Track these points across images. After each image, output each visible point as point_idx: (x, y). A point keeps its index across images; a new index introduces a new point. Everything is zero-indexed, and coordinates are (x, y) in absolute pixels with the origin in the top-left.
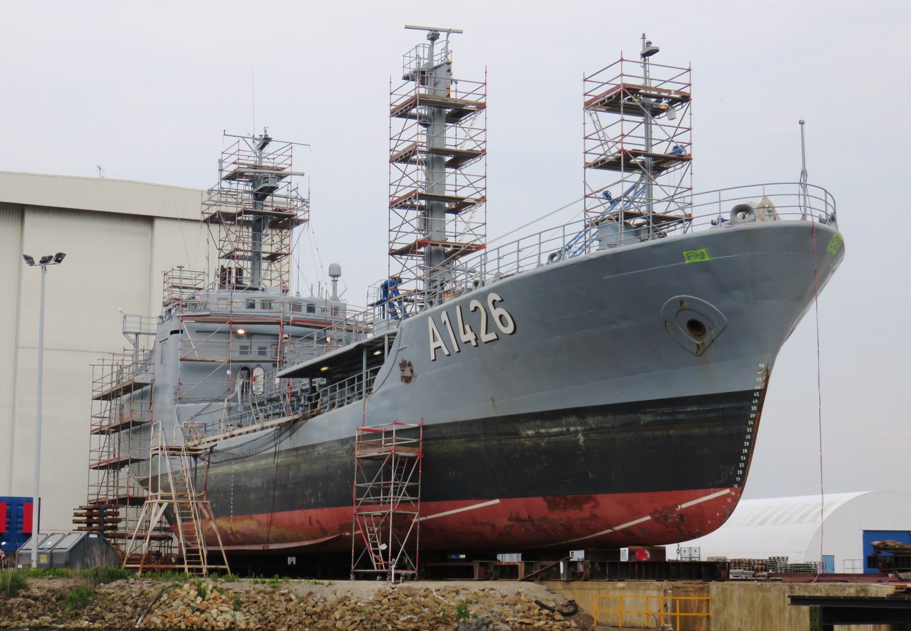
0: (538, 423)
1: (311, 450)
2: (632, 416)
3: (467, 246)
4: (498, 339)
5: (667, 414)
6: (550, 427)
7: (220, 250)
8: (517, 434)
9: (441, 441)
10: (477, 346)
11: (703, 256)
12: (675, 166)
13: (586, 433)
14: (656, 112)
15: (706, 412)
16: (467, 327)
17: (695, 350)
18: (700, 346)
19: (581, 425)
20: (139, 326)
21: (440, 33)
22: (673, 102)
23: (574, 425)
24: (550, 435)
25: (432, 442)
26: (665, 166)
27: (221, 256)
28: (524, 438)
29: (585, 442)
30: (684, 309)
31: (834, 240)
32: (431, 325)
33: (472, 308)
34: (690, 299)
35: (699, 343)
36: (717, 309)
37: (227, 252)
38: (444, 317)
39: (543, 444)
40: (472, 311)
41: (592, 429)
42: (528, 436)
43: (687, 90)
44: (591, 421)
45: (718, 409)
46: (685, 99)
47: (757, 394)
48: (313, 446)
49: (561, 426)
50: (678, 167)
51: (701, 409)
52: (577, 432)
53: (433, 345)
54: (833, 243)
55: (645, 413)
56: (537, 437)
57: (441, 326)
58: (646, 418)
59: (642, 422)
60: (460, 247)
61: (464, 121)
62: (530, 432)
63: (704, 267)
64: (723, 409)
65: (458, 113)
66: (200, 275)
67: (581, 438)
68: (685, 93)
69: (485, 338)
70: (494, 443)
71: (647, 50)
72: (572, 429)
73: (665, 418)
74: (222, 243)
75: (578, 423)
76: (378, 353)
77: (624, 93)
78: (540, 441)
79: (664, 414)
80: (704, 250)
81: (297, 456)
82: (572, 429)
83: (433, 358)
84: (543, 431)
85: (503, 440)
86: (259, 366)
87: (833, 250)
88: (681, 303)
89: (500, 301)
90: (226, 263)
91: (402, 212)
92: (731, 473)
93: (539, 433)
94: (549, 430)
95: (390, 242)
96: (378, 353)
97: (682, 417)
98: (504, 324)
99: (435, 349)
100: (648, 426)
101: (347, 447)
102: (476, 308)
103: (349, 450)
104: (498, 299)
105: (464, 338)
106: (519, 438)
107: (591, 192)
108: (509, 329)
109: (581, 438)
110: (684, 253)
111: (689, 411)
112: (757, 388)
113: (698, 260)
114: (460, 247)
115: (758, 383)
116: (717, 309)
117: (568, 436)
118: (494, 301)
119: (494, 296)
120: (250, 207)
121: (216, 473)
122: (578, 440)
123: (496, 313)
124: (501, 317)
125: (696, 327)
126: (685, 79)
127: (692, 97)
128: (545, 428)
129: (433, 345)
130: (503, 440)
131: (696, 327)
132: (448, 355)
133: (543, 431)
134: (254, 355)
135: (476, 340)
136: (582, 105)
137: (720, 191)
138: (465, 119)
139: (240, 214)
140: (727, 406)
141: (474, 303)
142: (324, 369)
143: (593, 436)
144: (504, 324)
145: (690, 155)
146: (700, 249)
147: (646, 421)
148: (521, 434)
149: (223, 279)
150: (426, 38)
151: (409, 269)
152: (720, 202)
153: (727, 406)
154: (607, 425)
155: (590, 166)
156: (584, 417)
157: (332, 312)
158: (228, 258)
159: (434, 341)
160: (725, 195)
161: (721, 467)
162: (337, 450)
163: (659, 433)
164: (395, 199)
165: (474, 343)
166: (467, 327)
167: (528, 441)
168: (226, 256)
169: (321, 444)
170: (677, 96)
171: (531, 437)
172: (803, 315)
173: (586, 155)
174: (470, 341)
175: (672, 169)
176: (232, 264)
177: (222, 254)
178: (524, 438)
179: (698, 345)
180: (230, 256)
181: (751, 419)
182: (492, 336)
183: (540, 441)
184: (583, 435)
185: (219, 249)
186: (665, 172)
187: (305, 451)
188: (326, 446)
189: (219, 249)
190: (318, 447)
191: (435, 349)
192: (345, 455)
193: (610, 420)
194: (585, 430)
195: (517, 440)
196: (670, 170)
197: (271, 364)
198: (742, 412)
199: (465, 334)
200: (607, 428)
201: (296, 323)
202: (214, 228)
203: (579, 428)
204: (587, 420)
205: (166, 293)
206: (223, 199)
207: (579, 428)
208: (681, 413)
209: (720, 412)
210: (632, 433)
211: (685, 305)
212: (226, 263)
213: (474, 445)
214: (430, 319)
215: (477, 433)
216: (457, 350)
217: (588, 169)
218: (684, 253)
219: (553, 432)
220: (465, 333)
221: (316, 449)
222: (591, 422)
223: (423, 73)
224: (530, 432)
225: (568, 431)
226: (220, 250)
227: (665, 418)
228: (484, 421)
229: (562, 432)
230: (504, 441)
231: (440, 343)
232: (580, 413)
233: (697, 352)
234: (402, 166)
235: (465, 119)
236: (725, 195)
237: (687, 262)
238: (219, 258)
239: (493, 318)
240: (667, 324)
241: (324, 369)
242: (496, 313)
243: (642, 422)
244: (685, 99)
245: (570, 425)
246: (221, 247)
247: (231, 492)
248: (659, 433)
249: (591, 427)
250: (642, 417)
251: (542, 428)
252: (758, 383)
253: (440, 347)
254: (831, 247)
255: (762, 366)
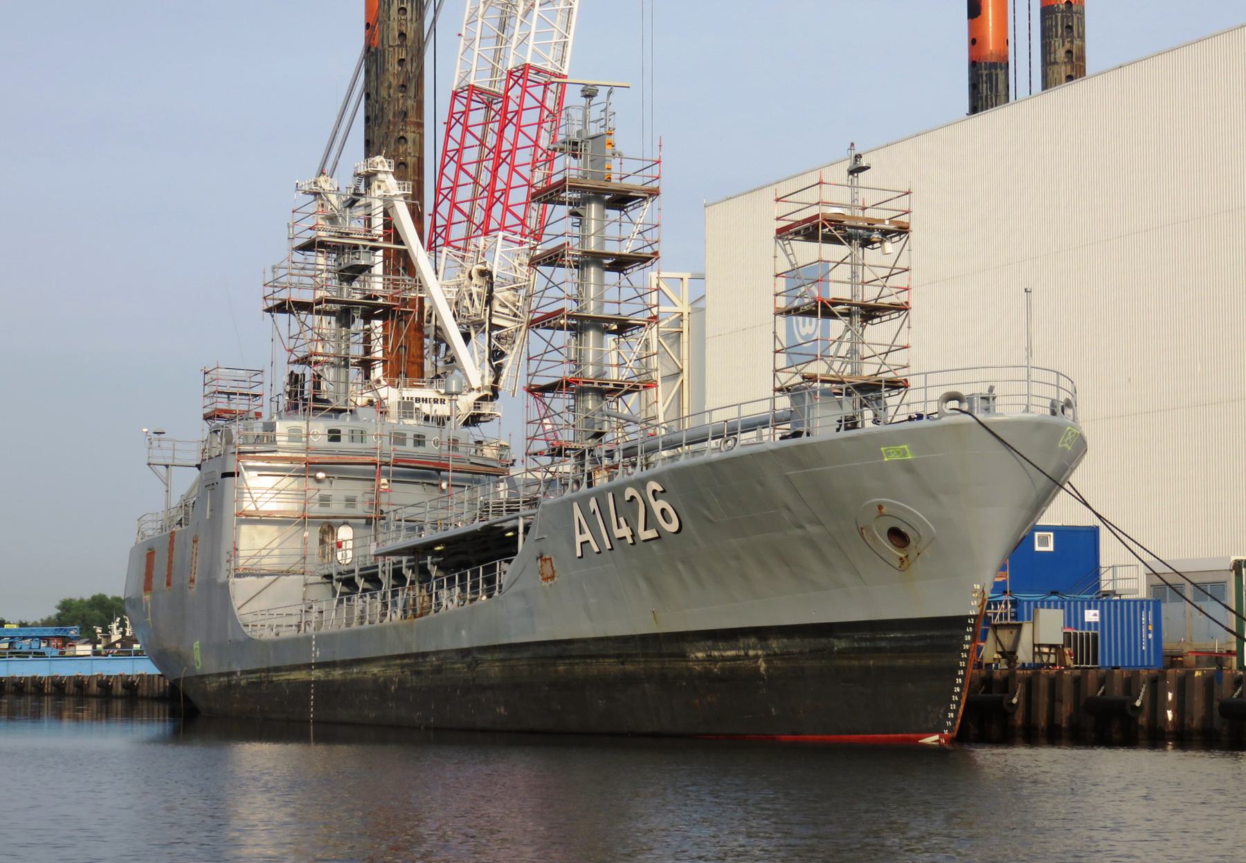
0: (710, 643)
1: (421, 660)
2: (824, 641)
3: (632, 384)
4: (659, 537)
5: (866, 640)
6: (725, 650)
7: (291, 351)
8: (683, 656)
9: (589, 661)
10: (634, 544)
11: (905, 454)
12: (890, 314)
13: (769, 658)
14: (866, 243)
15: (912, 639)
16: (622, 520)
17: (897, 564)
18: (904, 559)
19: (762, 648)
20: (172, 455)
21: (598, 87)
22: (885, 233)
23: (754, 648)
24: (724, 659)
25: (577, 661)
26: (878, 314)
27: (291, 360)
28: (693, 661)
29: (767, 670)
30: (882, 515)
31: (1067, 433)
32: (577, 513)
33: (627, 498)
34: (891, 504)
35: (902, 555)
36: (924, 518)
37: (301, 355)
38: (593, 505)
39: (716, 670)
40: (628, 501)
41: (775, 654)
42: (697, 660)
43: (905, 219)
44: (775, 644)
45: (926, 637)
46: (903, 230)
47: (971, 621)
48: (424, 655)
49: (739, 649)
50: (893, 316)
51: (906, 635)
52: (757, 657)
53: (579, 539)
54: (1065, 438)
55: (839, 638)
56: (708, 661)
57: (589, 516)
58: (840, 644)
59: (836, 649)
60: (623, 386)
61: (632, 207)
62: (700, 655)
63: (908, 467)
64: (931, 637)
65: (621, 200)
66: (256, 374)
67: (763, 666)
68: (903, 222)
69: (645, 535)
70: (656, 666)
71: (855, 167)
72: (751, 653)
73: (863, 644)
74: (293, 341)
75: (759, 646)
76: (510, 534)
77: (823, 224)
78: (712, 666)
79: (862, 640)
80: (905, 447)
81: (402, 666)
82: (751, 653)
83: (579, 554)
84: (716, 653)
85: (667, 663)
86: (345, 524)
87: (1067, 445)
88: (880, 507)
89: (661, 492)
90: (298, 369)
91: (547, 333)
92: (941, 716)
93: (710, 656)
94: (724, 654)
95: (529, 375)
96: (510, 534)
97: (883, 644)
98: (667, 519)
99: (582, 543)
100: (841, 652)
101: (469, 659)
102: (633, 498)
103: (471, 663)
104: (660, 489)
105: (618, 533)
106: (686, 661)
107: (781, 348)
108: (674, 527)
109: (763, 666)
110: (882, 449)
111: (891, 638)
112: (971, 613)
113: (898, 458)
114: (623, 386)
115: (972, 608)
116: (924, 518)
117: (746, 662)
118: (654, 492)
119: (654, 485)
120: (333, 295)
121: (289, 680)
122: (759, 667)
123: (657, 506)
124: (663, 511)
125: (898, 536)
126: (902, 203)
127: (912, 228)
128: (719, 650)
129: (579, 539)
130: (667, 663)
131: (898, 536)
132: (598, 553)
133: (716, 653)
134: (336, 508)
135: (633, 536)
136: (774, 233)
137: (926, 374)
138: (633, 205)
139: (319, 303)
140: (937, 633)
141: (630, 492)
142: (438, 548)
143: (777, 663)
144: (667, 519)
145: (907, 303)
146: (902, 444)
147: (840, 647)
148: (688, 656)
149: (293, 395)
150: (580, 94)
151: (557, 286)
152: (926, 387)
153: (937, 633)
154: (794, 650)
155: (781, 314)
156: (766, 639)
157: (449, 447)
158: (303, 363)
159: (580, 534)
160: (932, 379)
161: (929, 708)
162: (455, 663)
163: (855, 663)
164: (537, 316)
165: (630, 541)
166: (622, 520)
167: (698, 665)
168: (298, 361)
169: (436, 653)
170: (892, 227)
171: (701, 661)
172: (1043, 512)
173: (778, 297)
174: (625, 538)
175: (887, 318)
176: (309, 372)
177: (293, 358)
178: (693, 661)
179: (901, 559)
180: (304, 361)
181: (964, 651)
182: (651, 534)
183: (712, 666)
184: (765, 661)
185: (289, 350)
186: (876, 321)
187: (412, 661)
188: (442, 656)
189: (289, 350)
190: (431, 656)
191: (582, 543)
192: (466, 670)
193: (795, 645)
194: (768, 655)
195: (684, 663)
196: (884, 319)
197: (364, 521)
198: (954, 641)
199: (619, 528)
200: (793, 654)
201: (400, 464)
202: (282, 318)
203: (760, 652)
204: (770, 642)
205: (207, 401)
206: (295, 279)
207: (760, 652)
208: (882, 639)
209: (928, 641)
210: (823, 662)
211: (884, 510)
212: (298, 369)
213: (629, 667)
214: (575, 505)
215: (634, 652)
216: (609, 546)
217: (777, 317)
218: (882, 449)
219: (728, 656)
220: (619, 526)
221: (428, 659)
222: (774, 645)
223: (575, 144)
224: (700, 655)
225: (746, 654)
226: (291, 351)
227: (863, 644)
228: (644, 638)
229: (739, 656)
230: (667, 664)
231: (588, 536)
232: (761, 633)
233: (900, 567)
234: (547, 270)
235: (633, 205)
236: (932, 379)
237: (886, 459)
238: (288, 363)
239: (654, 512)
240: (864, 532)
241: (438, 548)
242: (657, 506)
243: (836, 649)
244: (903, 230)
245: (748, 647)
246: (291, 347)
247: (313, 706)
248: (855, 663)
249: (775, 652)
250: (836, 642)
251: (714, 650)
252: (972, 608)
253: (588, 541)
254: (1063, 442)
255: (978, 587)
